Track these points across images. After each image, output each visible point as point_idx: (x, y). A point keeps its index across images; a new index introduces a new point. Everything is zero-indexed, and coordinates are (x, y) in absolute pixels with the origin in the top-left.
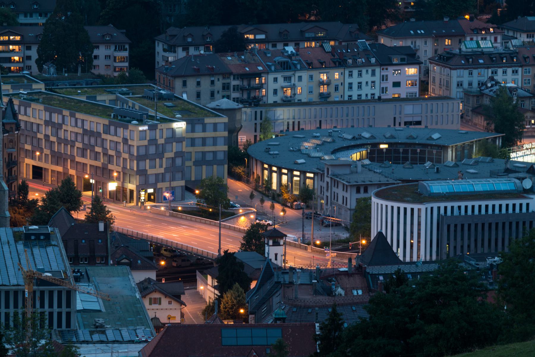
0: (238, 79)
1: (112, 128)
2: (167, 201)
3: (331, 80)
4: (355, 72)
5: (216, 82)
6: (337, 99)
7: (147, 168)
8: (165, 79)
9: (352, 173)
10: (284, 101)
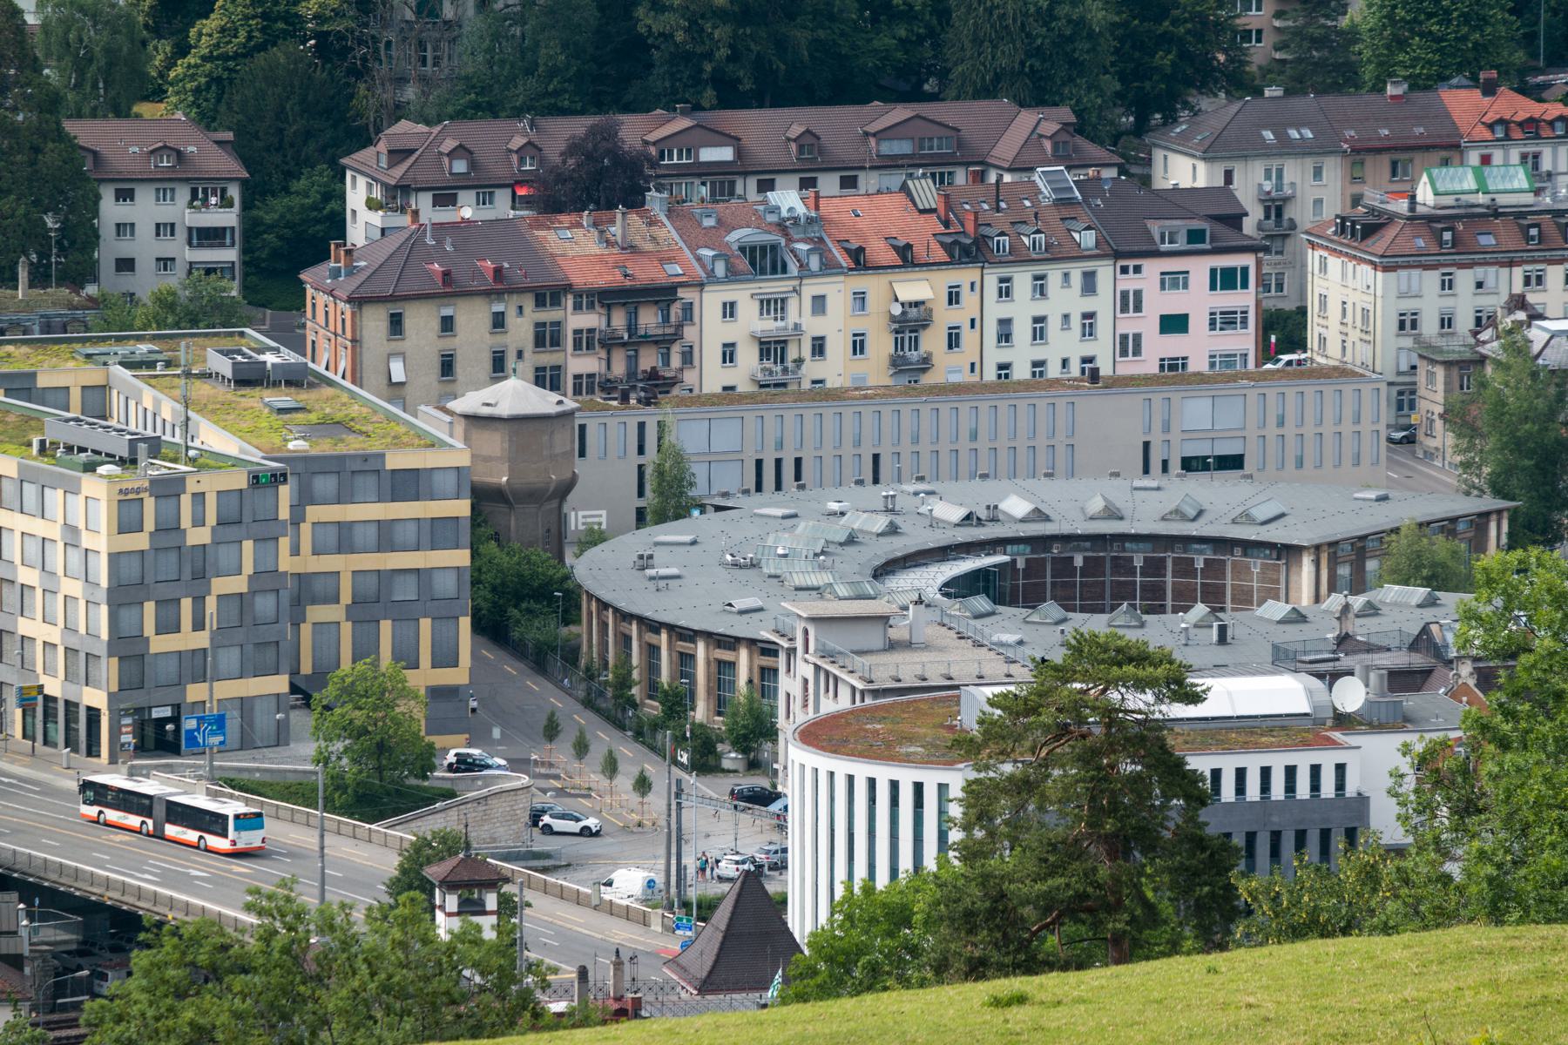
0: (591, 306)
1: (30, 491)
2: (195, 750)
3: (931, 310)
4: (1022, 280)
5: (511, 319)
6: (955, 378)
7: (149, 629)
8: (331, 309)
9: (892, 646)
10: (762, 386)
